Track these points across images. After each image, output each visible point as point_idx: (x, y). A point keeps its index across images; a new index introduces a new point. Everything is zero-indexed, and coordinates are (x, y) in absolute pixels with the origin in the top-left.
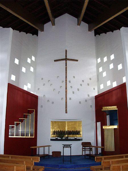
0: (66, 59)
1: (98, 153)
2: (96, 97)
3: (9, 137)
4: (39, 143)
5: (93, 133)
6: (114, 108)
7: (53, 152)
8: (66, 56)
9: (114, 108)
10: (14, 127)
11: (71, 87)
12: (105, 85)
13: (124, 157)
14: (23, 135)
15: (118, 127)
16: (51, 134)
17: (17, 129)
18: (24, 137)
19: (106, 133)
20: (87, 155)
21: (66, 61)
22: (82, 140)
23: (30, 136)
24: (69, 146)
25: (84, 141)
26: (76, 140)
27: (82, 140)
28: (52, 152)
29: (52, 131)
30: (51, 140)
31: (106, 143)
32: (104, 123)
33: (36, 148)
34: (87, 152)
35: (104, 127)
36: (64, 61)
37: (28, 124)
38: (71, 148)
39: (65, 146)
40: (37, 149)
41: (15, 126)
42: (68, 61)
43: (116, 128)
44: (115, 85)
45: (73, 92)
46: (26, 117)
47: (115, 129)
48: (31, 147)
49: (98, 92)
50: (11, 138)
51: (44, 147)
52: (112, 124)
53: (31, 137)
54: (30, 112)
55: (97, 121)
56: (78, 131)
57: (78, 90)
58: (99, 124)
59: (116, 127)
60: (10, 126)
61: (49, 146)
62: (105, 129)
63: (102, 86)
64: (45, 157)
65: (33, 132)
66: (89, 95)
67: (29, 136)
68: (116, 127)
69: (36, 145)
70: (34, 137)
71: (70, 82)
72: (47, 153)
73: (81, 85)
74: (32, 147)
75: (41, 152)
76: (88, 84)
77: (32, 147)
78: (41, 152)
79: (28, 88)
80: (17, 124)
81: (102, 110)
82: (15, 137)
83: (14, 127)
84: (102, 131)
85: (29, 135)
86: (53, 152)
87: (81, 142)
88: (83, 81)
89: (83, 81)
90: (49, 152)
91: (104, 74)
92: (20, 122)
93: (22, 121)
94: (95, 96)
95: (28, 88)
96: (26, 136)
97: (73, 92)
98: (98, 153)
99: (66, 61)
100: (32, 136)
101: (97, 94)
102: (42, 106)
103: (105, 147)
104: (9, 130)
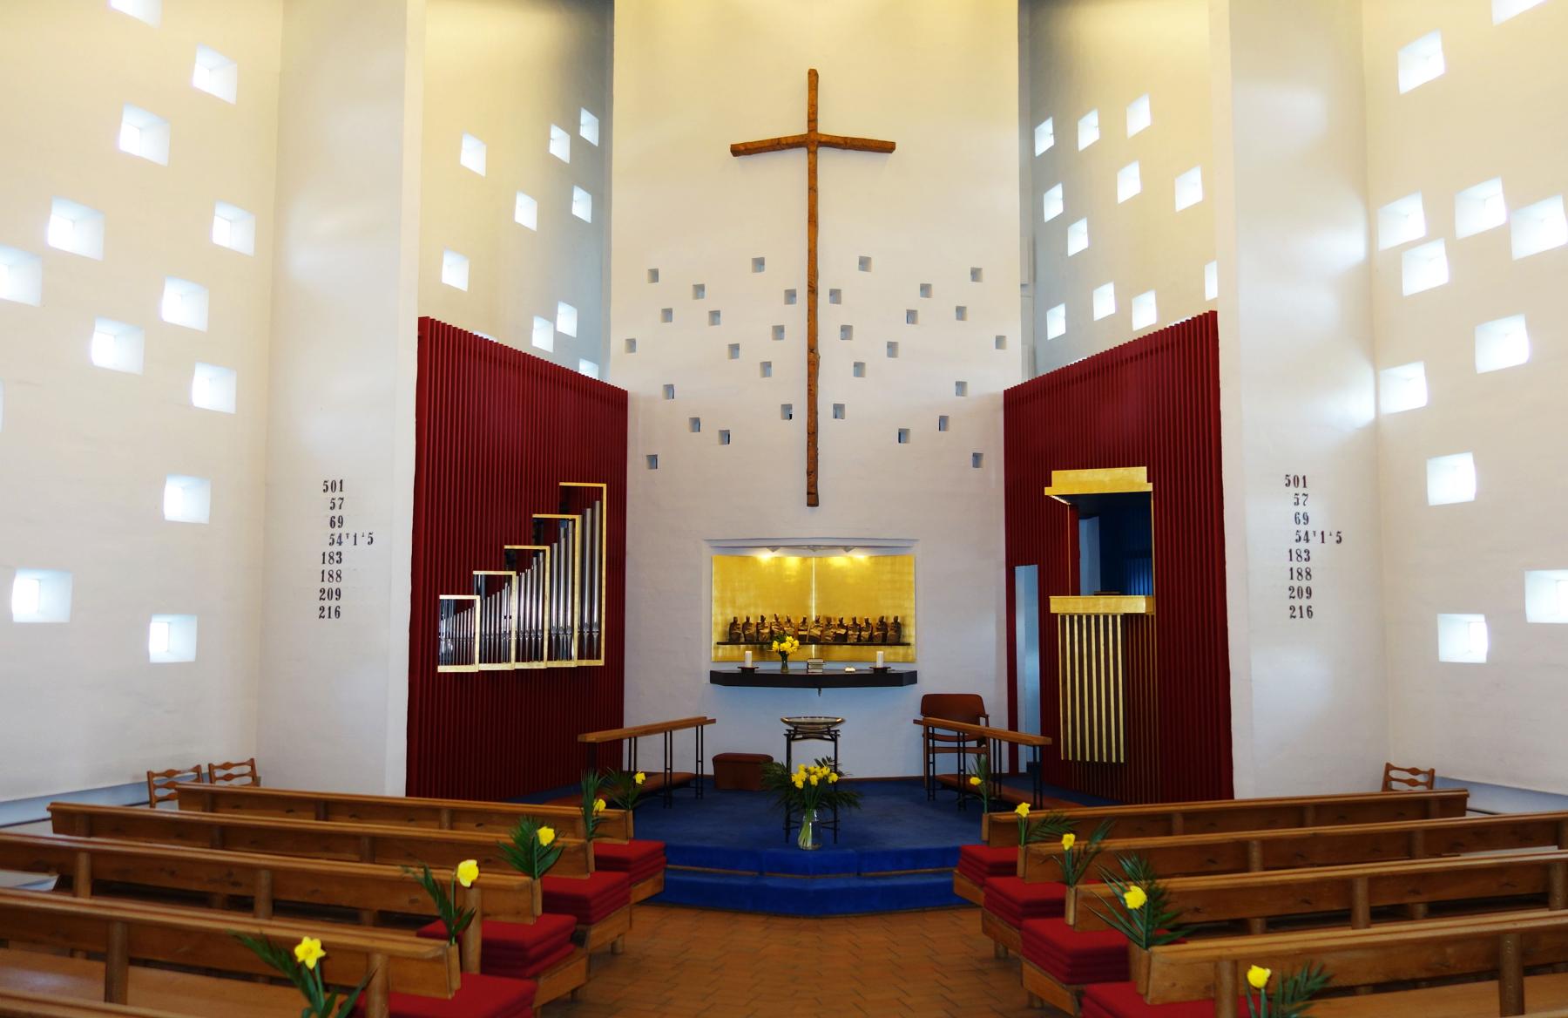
0: (812, 142)
1: (1023, 768)
2: (1015, 399)
3: (442, 669)
4: (636, 712)
5: (991, 632)
6: (1135, 479)
7: (717, 761)
8: (812, 120)
9: (1135, 479)
10: (471, 604)
11: (846, 331)
12: (1079, 314)
13: (1178, 823)
14: (529, 650)
15: (1153, 601)
16: (716, 638)
17: (493, 613)
18: (535, 665)
19: (1070, 643)
20: (944, 784)
21: (813, 154)
22: (911, 678)
23: (580, 657)
24: (827, 731)
25: (931, 683)
26: (882, 678)
27: (911, 678)
28: (713, 760)
29: (720, 618)
30: (718, 678)
31: (1068, 709)
32: (1057, 581)
33: (619, 742)
34: (946, 765)
35: (1058, 604)
36: (800, 157)
37: (555, 576)
38: (834, 739)
39: (798, 731)
40: (626, 742)
41: (477, 598)
42: (826, 157)
43: (1142, 615)
44: (1146, 317)
45: (859, 368)
46: (549, 533)
47: (1127, 618)
48: (581, 738)
49: (1033, 356)
50: (451, 674)
51: (668, 729)
52: (1114, 584)
53: (585, 663)
54: (577, 502)
55: (1014, 558)
56: (891, 620)
57: (892, 348)
58: (1027, 576)
59: (1138, 604)
60: (442, 597)
61: (700, 723)
62: (1063, 618)
63: (1056, 324)
64: (676, 793)
65: (595, 630)
66: (961, 387)
67: (570, 658)
68: (1138, 604)
69: (617, 720)
70: (601, 662)
71: (835, 295)
72: (684, 765)
73: (911, 316)
74: (592, 737)
75: (647, 760)
76: (961, 312)
77: (592, 737)
78: (647, 760)
79: (559, 338)
80: (494, 587)
81: (1048, 491)
82: (477, 667)
83: (471, 604)
84: (1048, 625)
85: (574, 652)
86: (717, 761)
87: (909, 700)
88: (925, 289)
89: (925, 289)
90: (700, 761)
91: (1078, 240)
92: (513, 573)
93: (521, 562)
94: (1007, 393)
95: (559, 338)
96: (550, 659)
97: (859, 368)
98: (1023, 768)
99: (813, 154)
100: (590, 657)
101: (1017, 377)
102: (653, 460)
103: (1066, 731)
104: (437, 627)
